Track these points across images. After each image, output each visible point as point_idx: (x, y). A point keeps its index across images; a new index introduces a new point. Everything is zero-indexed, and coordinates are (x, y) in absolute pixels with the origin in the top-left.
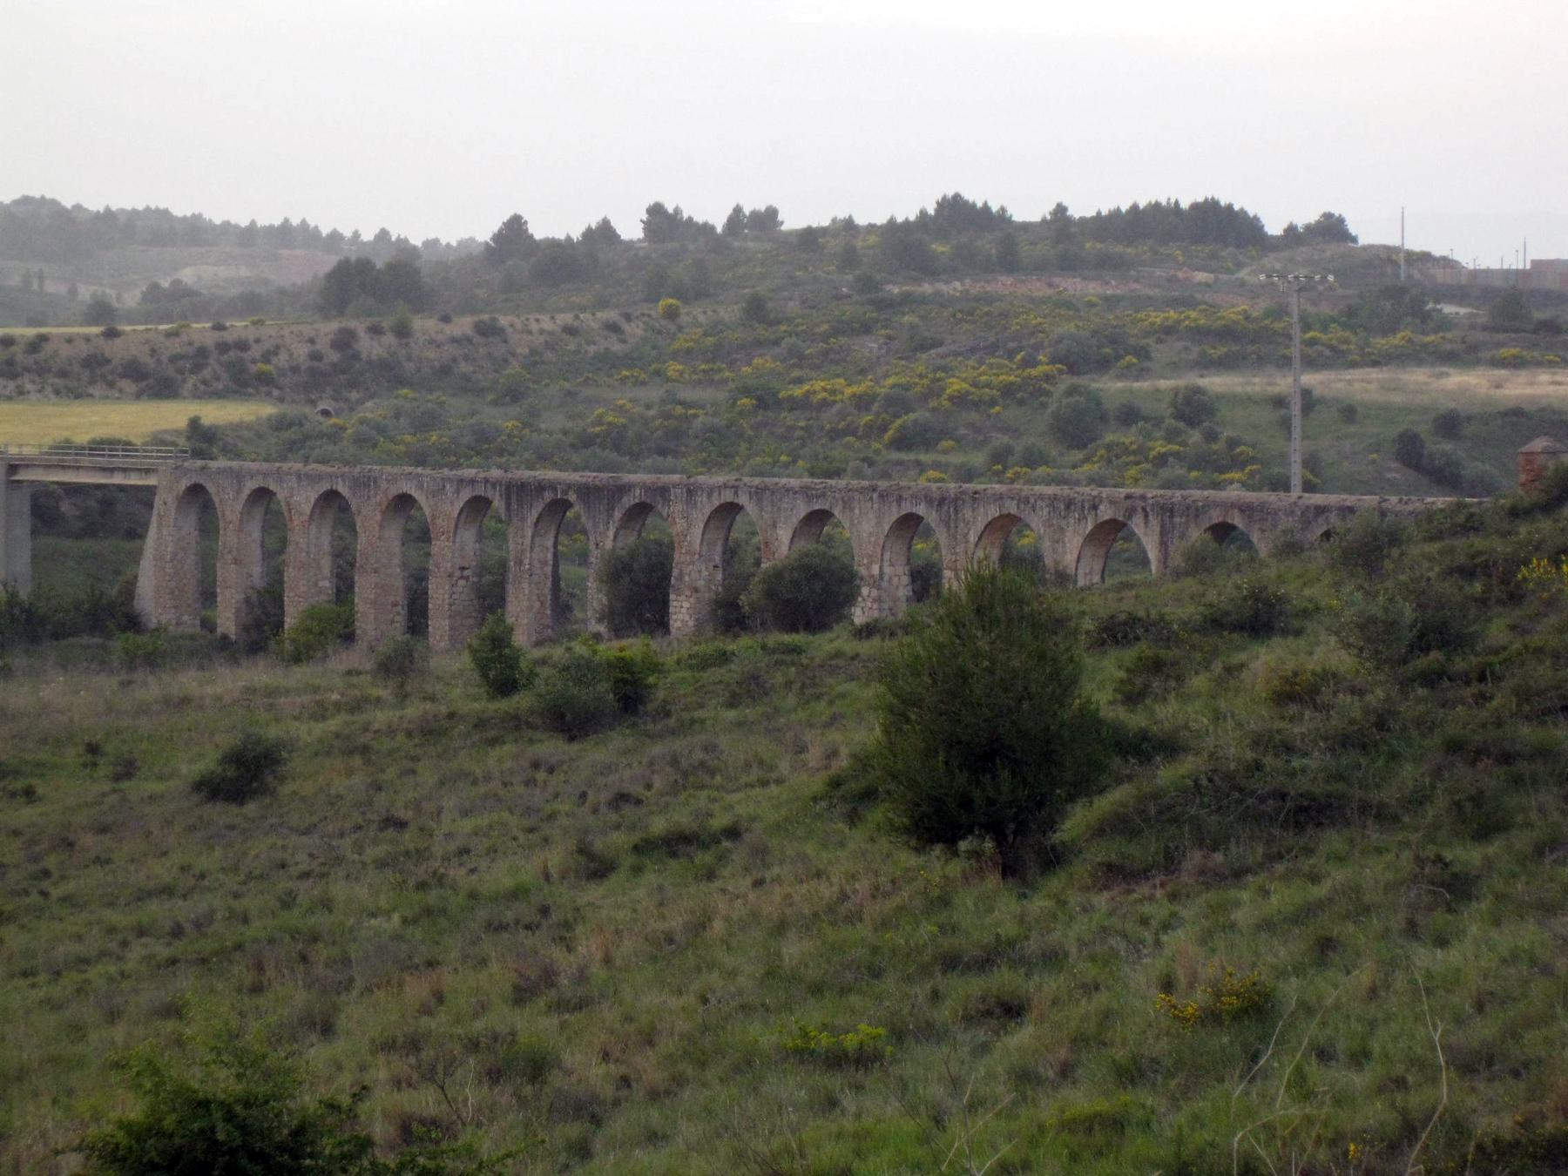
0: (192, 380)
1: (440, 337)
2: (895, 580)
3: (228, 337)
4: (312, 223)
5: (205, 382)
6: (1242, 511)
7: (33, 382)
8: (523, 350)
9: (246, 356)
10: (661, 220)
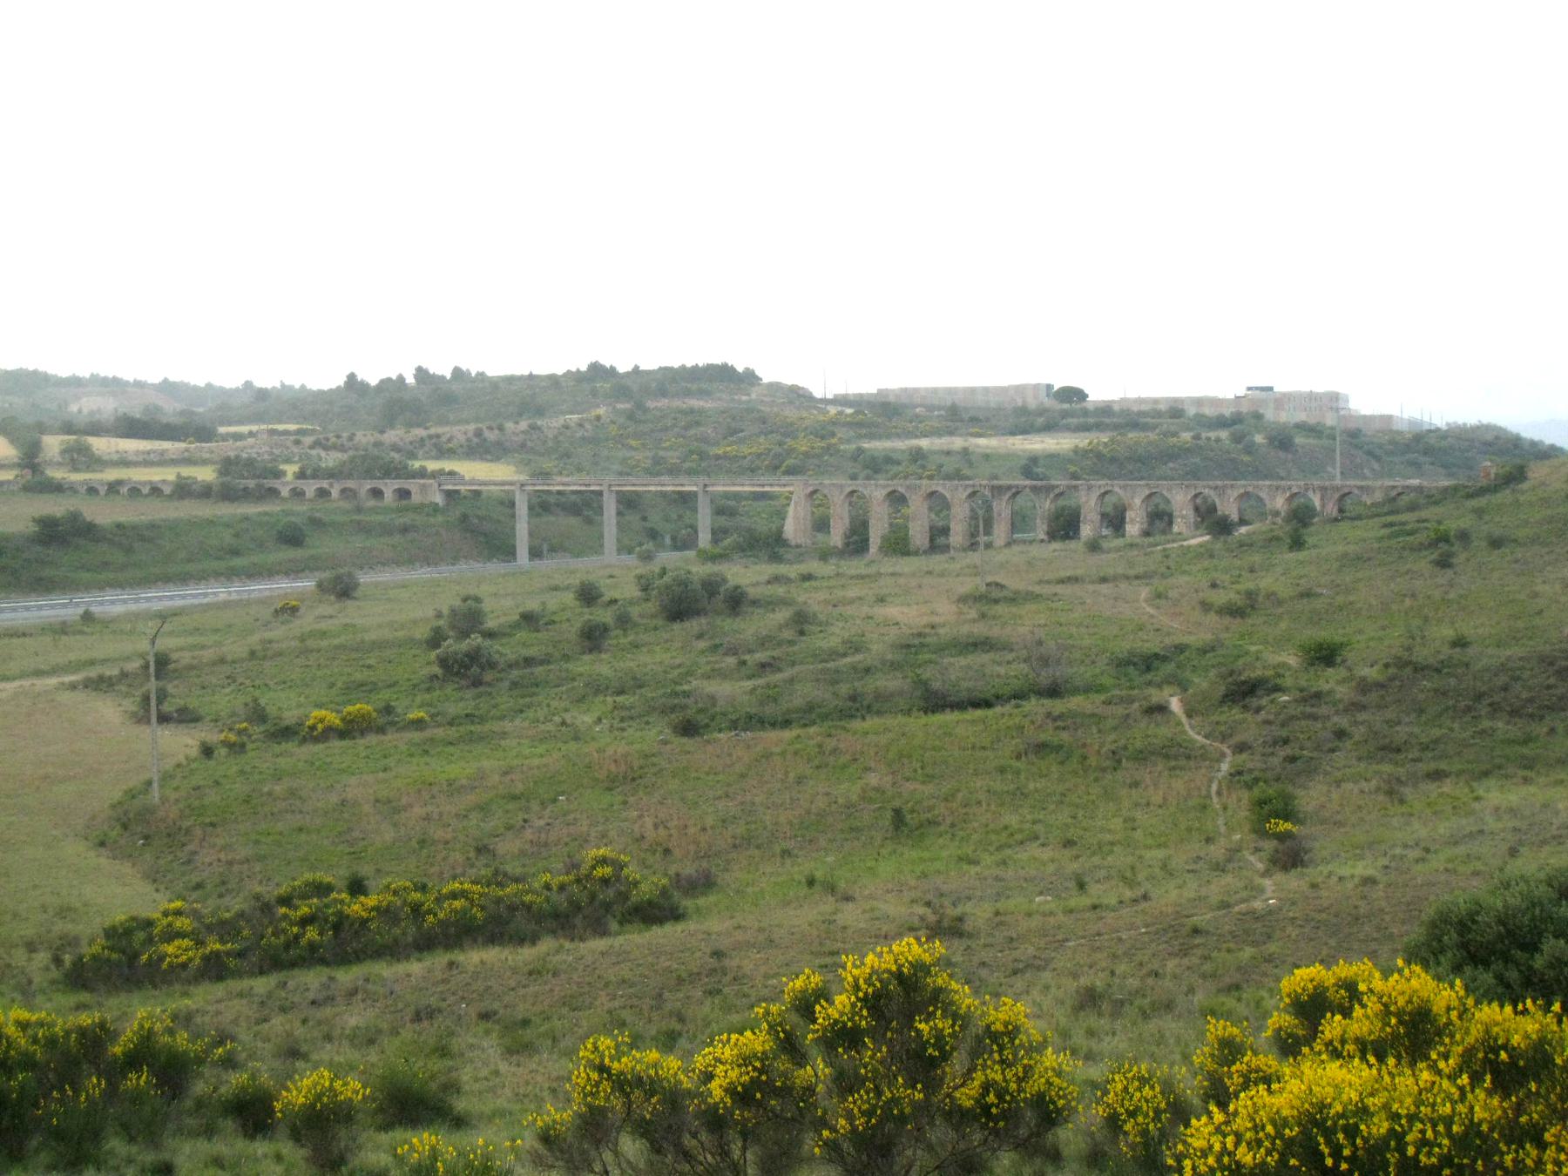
4: (287, 383)
8: (551, 436)
10: (457, 372)
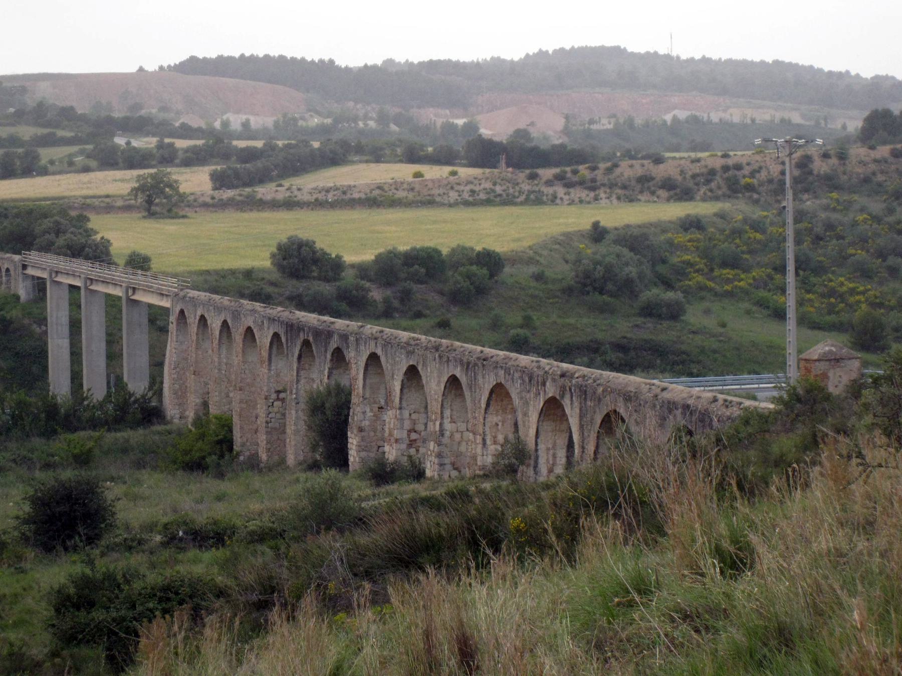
0: (703, 189)
1: (867, 159)
2: (457, 436)
3: (730, 162)
5: (711, 190)
7: (605, 192)
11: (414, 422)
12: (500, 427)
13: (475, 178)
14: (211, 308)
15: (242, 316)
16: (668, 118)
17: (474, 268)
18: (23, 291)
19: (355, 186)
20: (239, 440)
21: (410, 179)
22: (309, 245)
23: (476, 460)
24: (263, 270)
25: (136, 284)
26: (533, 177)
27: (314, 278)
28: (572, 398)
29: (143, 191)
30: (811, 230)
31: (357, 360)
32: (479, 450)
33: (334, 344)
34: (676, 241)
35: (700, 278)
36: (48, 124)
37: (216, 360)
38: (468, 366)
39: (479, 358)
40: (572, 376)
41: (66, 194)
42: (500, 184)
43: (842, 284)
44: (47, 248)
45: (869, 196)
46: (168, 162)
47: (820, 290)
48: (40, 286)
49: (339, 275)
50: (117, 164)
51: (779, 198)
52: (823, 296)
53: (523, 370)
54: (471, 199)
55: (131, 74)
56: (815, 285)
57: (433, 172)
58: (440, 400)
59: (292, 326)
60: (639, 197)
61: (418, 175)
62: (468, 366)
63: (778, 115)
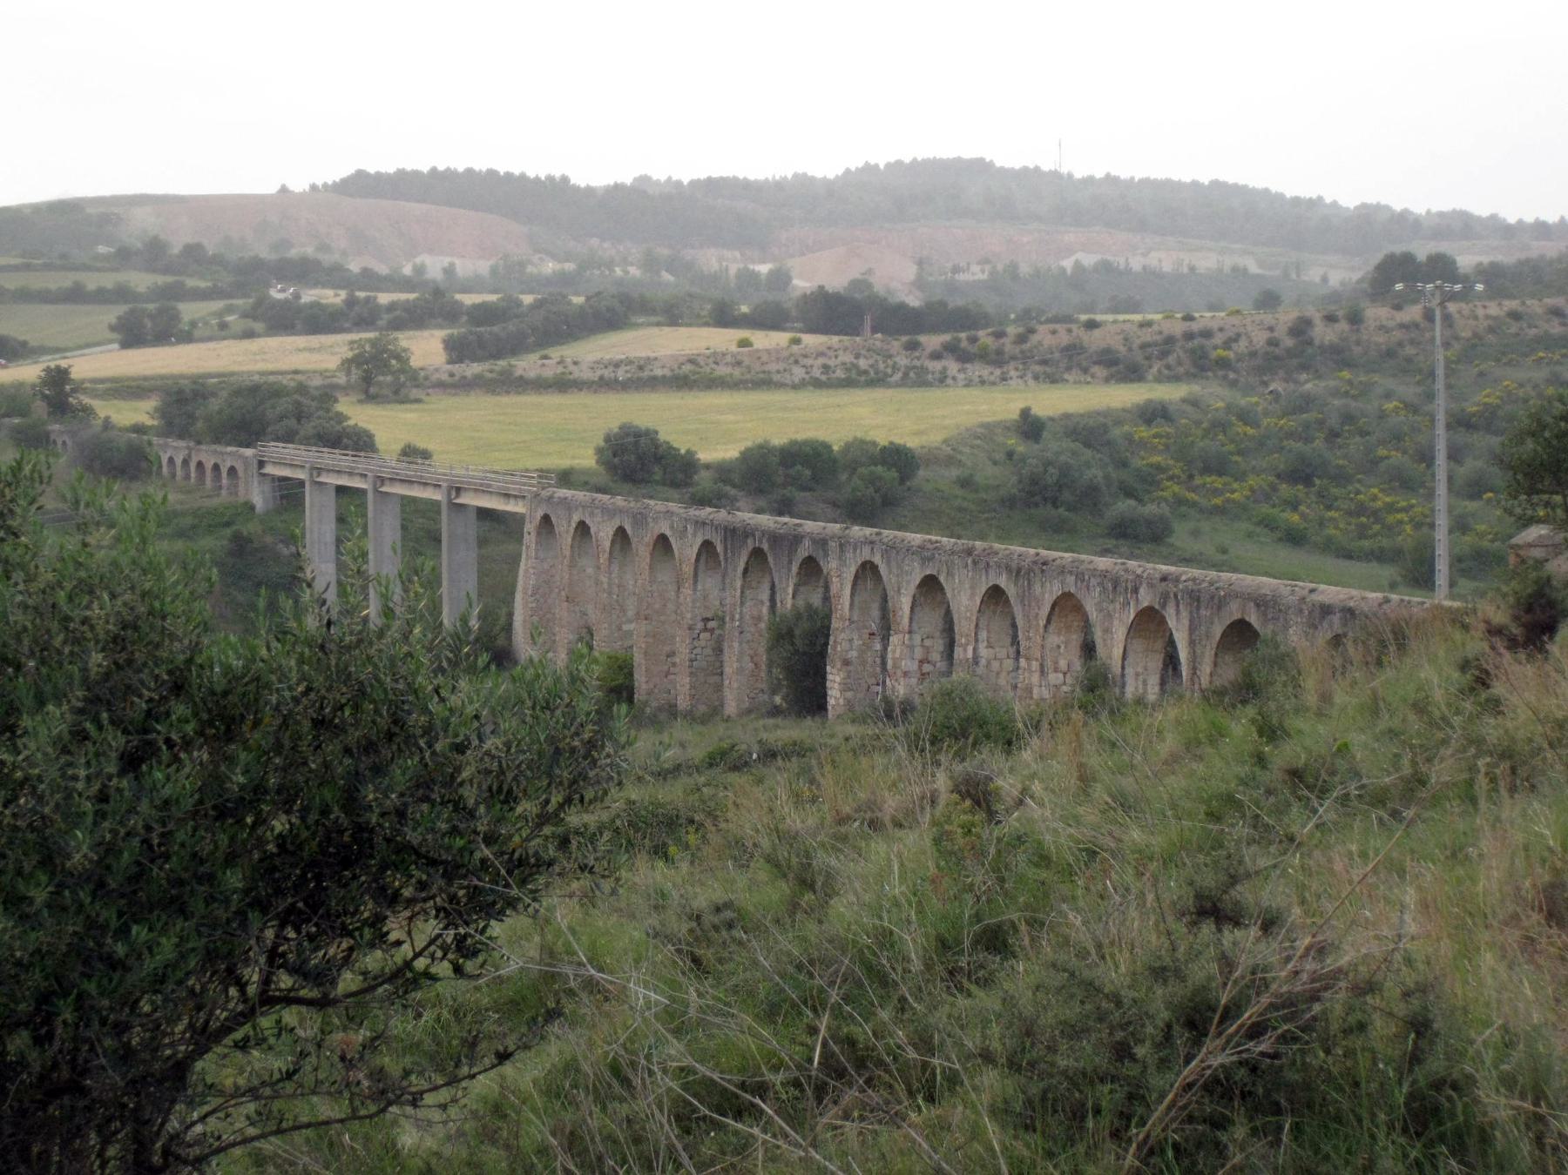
1: (1391, 324)
2: (995, 665)
3: (1194, 327)
5: (1168, 367)
6: (1258, 605)
7: (1017, 369)
9: (1208, 343)
11: (927, 650)
12: (1062, 650)
13: (829, 348)
14: (596, 511)
15: (650, 520)
16: (1068, 264)
17: (880, 468)
18: (259, 497)
19: (656, 359)
20: (644, 686)
21: (734, 348)
22: (650, 434)
23: (1031, 692)
24: (585, 471)
25: (462, 482)
26: (912, 346)
27: (657, 483)
28: (1178, 606)
29: (359, 365)
30: (1321, 422)
31: (841, 575)
32: (1035, 679)
33: (803, 551)
34: (1136, 437)
35: (1176, 488)
36: (166, 271)
37: (605, 580)
38: (1017, 573)
39: (1035, 563)
40: (1177, 580)
41: (236, 368)
42: (865, 357)
43: (1374, 498)
44: (289, 437)
45: (1394, 376)
46: (367, 324)
47: (1345, 505)
48: (289, 494)
49: (691, 477)
50: (293, 326)
51: (1265, 378)
52: (1349, 513)
53: (1104, 575)
54: (824, 378)
55: (272, 195)
56: (1336, 499)
57: (766, 340)
58: (974, 618)
59: (734, 530)
60: (1066, 376)
61: (744, 343)
62: (1017, 573)
63: (1229, 262)
